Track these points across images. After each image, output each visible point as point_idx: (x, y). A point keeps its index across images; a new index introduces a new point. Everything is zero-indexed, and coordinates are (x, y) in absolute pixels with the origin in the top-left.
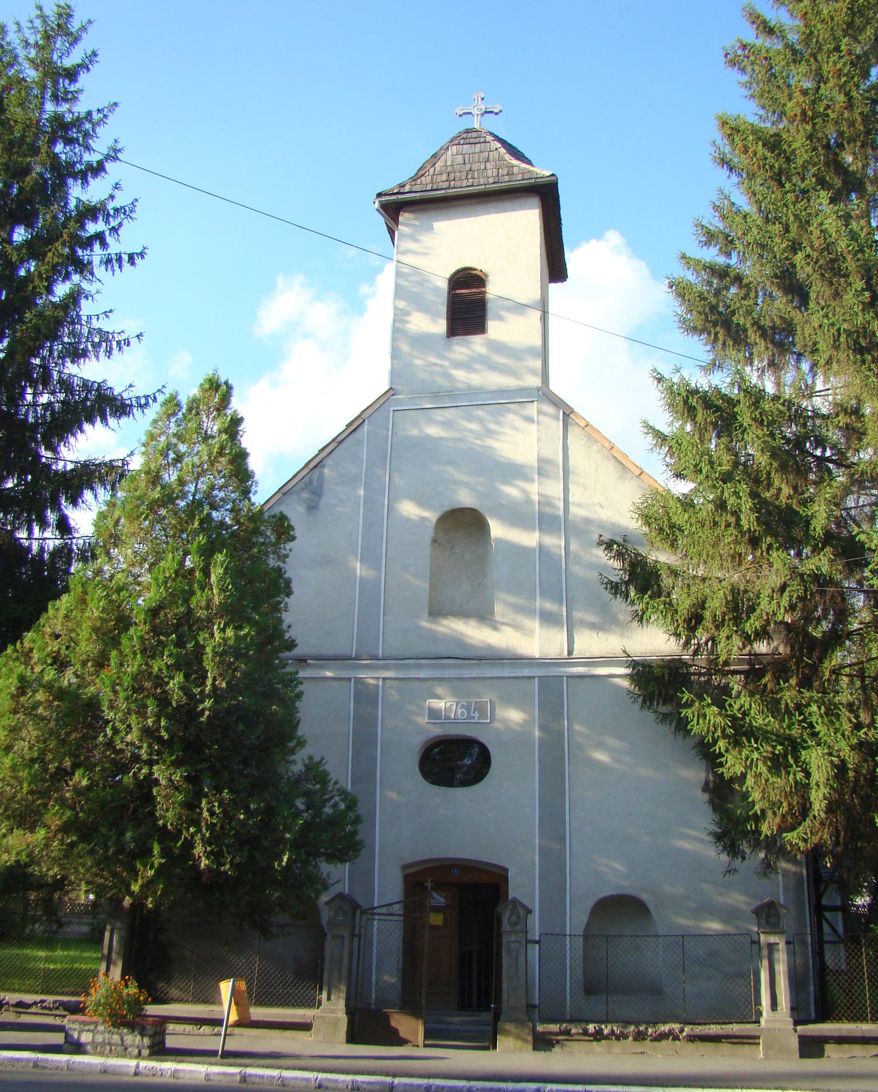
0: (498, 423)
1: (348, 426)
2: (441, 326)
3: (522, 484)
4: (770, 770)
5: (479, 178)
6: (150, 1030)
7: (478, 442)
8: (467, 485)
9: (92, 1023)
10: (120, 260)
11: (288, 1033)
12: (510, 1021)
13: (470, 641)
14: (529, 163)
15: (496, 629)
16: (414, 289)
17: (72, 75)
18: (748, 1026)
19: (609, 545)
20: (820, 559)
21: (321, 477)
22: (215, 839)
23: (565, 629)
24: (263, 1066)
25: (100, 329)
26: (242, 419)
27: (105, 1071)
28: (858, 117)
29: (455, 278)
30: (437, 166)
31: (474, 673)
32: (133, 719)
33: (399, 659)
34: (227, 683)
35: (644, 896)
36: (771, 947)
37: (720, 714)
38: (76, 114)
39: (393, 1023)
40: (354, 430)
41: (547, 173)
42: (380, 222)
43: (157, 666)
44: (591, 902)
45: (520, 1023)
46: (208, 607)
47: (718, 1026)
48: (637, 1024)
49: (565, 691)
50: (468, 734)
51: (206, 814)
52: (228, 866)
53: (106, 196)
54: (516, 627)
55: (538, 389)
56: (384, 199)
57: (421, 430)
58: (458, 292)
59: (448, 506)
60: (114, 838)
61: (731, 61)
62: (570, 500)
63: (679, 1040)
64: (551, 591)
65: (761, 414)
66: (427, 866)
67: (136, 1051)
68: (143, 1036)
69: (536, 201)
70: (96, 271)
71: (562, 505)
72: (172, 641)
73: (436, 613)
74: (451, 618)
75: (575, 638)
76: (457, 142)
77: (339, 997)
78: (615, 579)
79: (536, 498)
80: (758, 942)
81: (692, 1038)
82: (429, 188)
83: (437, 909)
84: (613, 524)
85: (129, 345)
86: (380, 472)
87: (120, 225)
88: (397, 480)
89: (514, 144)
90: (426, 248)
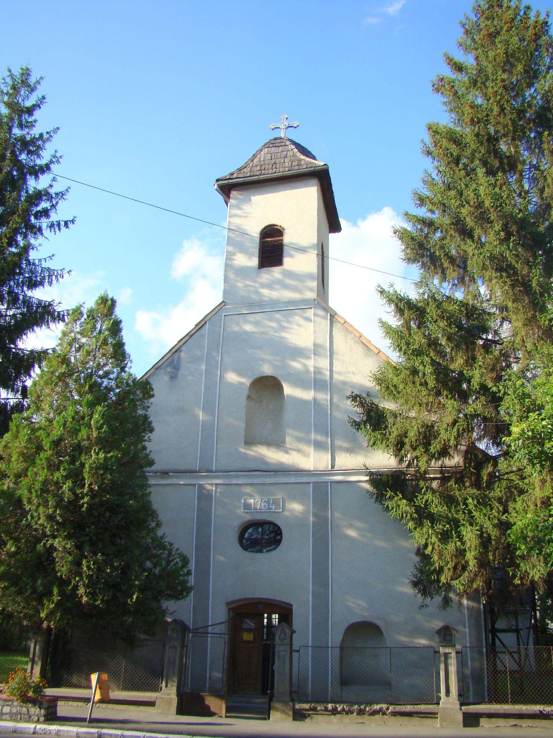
0: (288, 322)
1: (197, 325)
2: (255, 262)
3: (303, 360)
4: (440, 540)
5: (279, 168)
6: (45, 704)
7: (276, 334)
8: (269, 362)
9: (10, 700)
10: (59, 225)
11: (142, 708)
12: (280, 702)
13: (269, 460)
14: (314, 158)
15: (287, 452)
16: (238, 239)
17: (30, 111)
18: (431, 706)
19: (354, 398)
20: (477, 405)
21: (179, 358)
22: (92, 584)
23: (330, 452)
24: (113, 728)
25: (48, 268)
26: (121, 321)
27: (15, 731)
28: (508, 121)
29: (264, 231)
30: (254, 161)
31: (272, 480)
32: (41, 509)
33: (226, 472)
34: (98, 487)
35: (378, 622)
36: (446, 655)
37: (409, 505)
38: (33, 135)
39: (207, 702)
40: (200, 328)
41: (322, 164)
42: (220, 198)
43: (57, 475)
44: (345, 626)
45: (284, 702)
46: (88, 438)
47: (412, 706)
48: (360, 704)
49: (329, 492)
50: (268, 519)
51: (85, 569)
52: (99, 602)
53: (48, 186)
54: (298, 451)
55: (315, 300)
56: (220, 183)
57: (241, 328)
58: (266, 239)
59: (257, 375)
60: (30, 584)
61: (436, 89)
62: (334, 370)
63: (386, 715)
64: (321, 429)
65: (442, 312)
66: (241, 603)
67: (36, 718)
68: (40, 708)
69: (315, 182)
70: (44, 232)
71: (328, 373)
72: (66, 461)
73: (250, 442)
74: (259, 446)
75: (336, 457)
76: (268, 146)
77: (173, 685)
78: (358, 420)
79: (312, 369)
80: (438, 652)
81: (395, 714)
82: (248, 175)
83: (249, 630)
84: (361, 385)
85: (63, 277)
86: (215, 354)
87: (57, 203)
88: (226, 360)
89: (305, 146)
90: (247, 213)
